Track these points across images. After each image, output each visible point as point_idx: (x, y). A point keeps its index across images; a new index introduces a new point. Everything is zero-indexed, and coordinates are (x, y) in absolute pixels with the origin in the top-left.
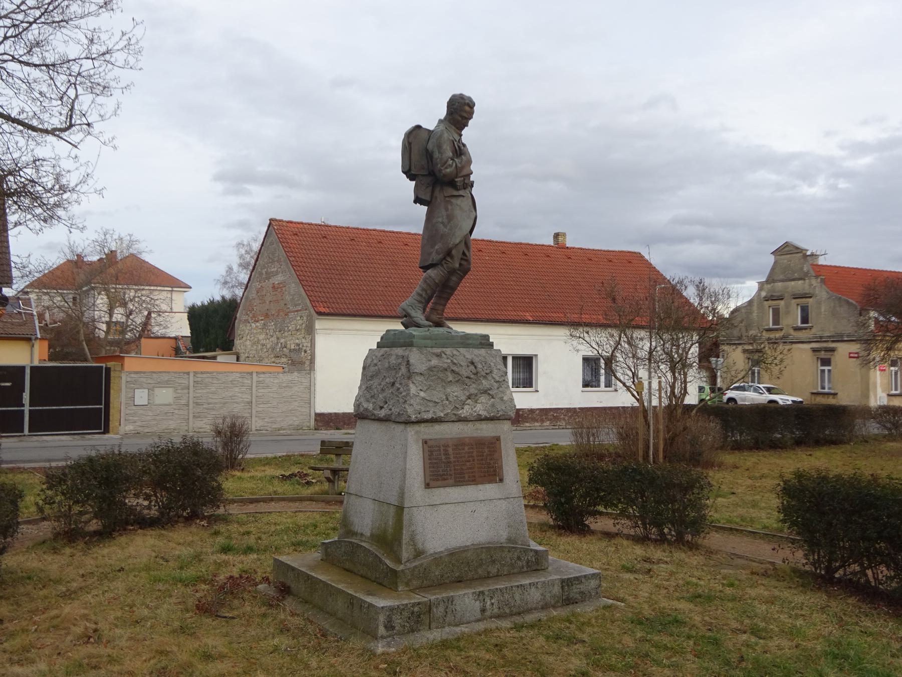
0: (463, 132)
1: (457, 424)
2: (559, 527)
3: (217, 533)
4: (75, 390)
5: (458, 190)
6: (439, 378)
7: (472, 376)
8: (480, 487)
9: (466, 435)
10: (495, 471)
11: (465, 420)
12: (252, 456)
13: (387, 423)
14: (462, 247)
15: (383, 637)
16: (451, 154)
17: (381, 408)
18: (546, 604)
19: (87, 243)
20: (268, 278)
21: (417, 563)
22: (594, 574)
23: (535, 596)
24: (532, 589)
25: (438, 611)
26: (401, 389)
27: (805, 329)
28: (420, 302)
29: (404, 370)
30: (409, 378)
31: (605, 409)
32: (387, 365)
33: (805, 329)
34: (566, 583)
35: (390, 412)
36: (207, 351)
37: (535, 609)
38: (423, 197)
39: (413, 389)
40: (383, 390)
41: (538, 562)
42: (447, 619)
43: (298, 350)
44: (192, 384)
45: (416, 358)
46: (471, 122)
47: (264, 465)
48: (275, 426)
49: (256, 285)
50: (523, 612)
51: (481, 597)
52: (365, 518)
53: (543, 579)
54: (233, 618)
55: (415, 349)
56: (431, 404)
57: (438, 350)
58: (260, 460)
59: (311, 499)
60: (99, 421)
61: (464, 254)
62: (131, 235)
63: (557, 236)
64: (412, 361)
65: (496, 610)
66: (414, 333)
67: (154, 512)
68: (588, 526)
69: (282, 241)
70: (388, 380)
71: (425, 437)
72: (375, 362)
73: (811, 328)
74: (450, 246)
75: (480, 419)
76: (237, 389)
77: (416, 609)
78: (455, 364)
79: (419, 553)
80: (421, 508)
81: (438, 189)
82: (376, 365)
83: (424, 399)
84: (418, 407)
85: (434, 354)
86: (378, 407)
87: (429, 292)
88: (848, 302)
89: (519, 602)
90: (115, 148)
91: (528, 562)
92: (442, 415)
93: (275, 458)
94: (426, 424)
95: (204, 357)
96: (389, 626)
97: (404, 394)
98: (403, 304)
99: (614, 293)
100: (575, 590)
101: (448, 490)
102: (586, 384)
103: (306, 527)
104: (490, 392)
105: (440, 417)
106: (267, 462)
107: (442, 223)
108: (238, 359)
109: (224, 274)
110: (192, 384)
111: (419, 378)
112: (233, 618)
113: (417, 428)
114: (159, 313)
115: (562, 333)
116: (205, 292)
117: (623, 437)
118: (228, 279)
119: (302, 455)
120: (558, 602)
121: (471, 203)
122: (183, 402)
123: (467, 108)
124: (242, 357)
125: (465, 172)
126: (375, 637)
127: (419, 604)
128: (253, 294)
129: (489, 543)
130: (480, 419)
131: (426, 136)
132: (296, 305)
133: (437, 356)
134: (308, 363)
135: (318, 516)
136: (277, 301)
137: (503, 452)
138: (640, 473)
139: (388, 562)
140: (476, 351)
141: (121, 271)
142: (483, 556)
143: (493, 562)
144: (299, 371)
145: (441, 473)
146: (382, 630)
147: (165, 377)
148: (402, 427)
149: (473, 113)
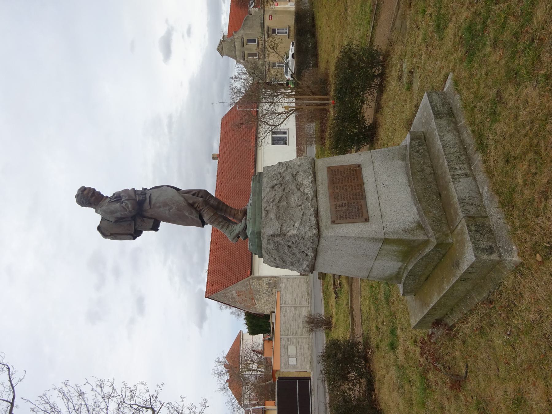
0: (105, 195)
1: (319, 198)
2: (372, 141)
3: (378, 347)
4: (291, 394)
5: (146, 199)
6: (284, 212)
7: (283, 187)
8: (365, 180)
9: (327, 192)
10: (353, 170)
11: (316, 192)
12: (323, 311)
13: (319, 251)
14: (189, 195)
15: (500, 256)
16: (118, 204)
17: (307, 255)
18: (455, 129)
19: (219, 382)
20: (234, 298)
21: (429, 228)
22: (428, 97)
23: (449, 137)
24: (442, 140)
25: (472, 210)
26: (293, 241)
27: (258, 41)
28: (228, 227)
29: (278, 239)
30: (285, 235)
31: (297, 134)
32: (275, 251)
33: (258, 41)
34: (437, 115)
35: (311, 249)
36: (270, 326)
37: (460, 137)
38: (151, 224)
39: (293, 232)
40: (294, 254)
41: (419, 138)
42: (477, 203)
43: (269, 284)
44: (286, 337)
45: (269, 230)
46: (97, 190)
47: (329, 305)
48: (306, 295)
49: (237, 304)
50: (463, 146)
51: (457, 177)
52: (389, 265)
53: (436, 132)
54: (467, 367)
55: (262, 231)
56: (305, 218)
57: (264, 213)
58: (326, 307)
59: (351, 285)
60: (304, 383)
61: (194, 195)
62: (216, 361)
63: (213, 158)
64: (271, 233)
65: (465, 166)
66: (251, 231)
67: (363, 381)
68: (371, 124)
69: (216, 291)
70: (286, 251)
71: (329, 222)
72: (272, 260)
73: (258, 38)
74: (186, 204)
75: (315, 181)
76: (289, 314)
77: (473, 228)
78: (274, 200)
79: (420, 226)
80: (385, 225)
81: (146, 214)
82: (275, 259)
83: (300, 223)
84: (307, 228)
85: (266, 216)
86: (306, 258)
87: (220, 220)
88: (246, 20)
89: (456, 149)
90: (163, 384)
91: (419, 145)
92: (312, 209)
93: (324, 299)
94: (320, 222)
95: (273, 328)
96: (490, 250)
97: (297, 239)
98: (230, 239)
99: (240, 128)
100: (443, 110)
101: (369, 204)
102: (285, 144)
103: (372, 292)
104: (295, 174)
105: (314, 211)
106: (327, 304)
107: (169, 210)
108: (274, 312)
109: (234, 316)
110: (286, 337)
111: (285, 227)
112: (467, 367)
113: (323, 229)
114: (252, 347)
115: (260, 151)
116: (241, 325)
117: (312, 120)
118: (237, 314)
119: (323, 285)
120: (452, 121)
121: (156, 190)
122: (295, 340)
123: (85, 192)
124: (273, 310)
125: (132, 194)
126: (500, 262)
127: (468, 226)
128: (242, 306)
129: (407, 174)
130: (315, 181)
131: (106, 222)
132: (247, 285)
133: (268, 213)
134: (275, 279)
135: (364, 283)
136: (245, 294)
137: (338, 164)
138: (341, 88)
139: (427, 250)
140: (264, 184)
141: (234, 364)
142: (419, 177)
143: (422, 170)
144: (279, 283)
145: (356, 210)
146: (494, 257)
147: (283, 349)
148: (322, 240)
149: (90, 188)
